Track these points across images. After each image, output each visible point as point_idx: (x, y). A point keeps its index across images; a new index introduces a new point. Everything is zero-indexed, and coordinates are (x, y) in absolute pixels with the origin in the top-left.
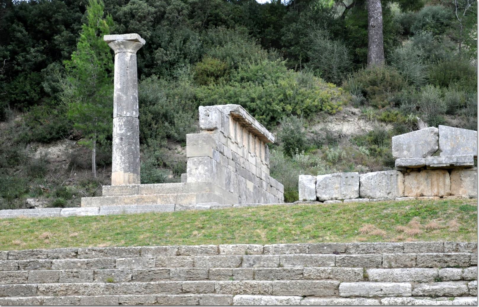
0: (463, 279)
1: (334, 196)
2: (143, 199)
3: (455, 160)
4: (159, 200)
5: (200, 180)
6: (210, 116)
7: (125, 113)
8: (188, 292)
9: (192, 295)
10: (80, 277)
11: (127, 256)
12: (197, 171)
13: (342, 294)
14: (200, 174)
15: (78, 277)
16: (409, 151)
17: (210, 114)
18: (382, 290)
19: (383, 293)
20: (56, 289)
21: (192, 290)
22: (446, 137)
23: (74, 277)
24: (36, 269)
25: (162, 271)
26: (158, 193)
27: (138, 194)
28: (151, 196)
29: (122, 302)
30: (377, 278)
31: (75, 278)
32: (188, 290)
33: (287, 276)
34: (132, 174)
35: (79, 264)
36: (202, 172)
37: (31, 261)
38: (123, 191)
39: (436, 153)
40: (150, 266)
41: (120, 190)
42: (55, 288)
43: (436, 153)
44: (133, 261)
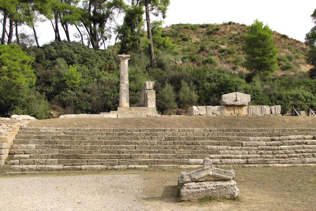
0: (279, 140)
2: (133, 112)
9: (190, 146)
18: (256, 144)
21: (191, 144)
27: (131, 110)
39: (236, 101)
43: (236, 101)
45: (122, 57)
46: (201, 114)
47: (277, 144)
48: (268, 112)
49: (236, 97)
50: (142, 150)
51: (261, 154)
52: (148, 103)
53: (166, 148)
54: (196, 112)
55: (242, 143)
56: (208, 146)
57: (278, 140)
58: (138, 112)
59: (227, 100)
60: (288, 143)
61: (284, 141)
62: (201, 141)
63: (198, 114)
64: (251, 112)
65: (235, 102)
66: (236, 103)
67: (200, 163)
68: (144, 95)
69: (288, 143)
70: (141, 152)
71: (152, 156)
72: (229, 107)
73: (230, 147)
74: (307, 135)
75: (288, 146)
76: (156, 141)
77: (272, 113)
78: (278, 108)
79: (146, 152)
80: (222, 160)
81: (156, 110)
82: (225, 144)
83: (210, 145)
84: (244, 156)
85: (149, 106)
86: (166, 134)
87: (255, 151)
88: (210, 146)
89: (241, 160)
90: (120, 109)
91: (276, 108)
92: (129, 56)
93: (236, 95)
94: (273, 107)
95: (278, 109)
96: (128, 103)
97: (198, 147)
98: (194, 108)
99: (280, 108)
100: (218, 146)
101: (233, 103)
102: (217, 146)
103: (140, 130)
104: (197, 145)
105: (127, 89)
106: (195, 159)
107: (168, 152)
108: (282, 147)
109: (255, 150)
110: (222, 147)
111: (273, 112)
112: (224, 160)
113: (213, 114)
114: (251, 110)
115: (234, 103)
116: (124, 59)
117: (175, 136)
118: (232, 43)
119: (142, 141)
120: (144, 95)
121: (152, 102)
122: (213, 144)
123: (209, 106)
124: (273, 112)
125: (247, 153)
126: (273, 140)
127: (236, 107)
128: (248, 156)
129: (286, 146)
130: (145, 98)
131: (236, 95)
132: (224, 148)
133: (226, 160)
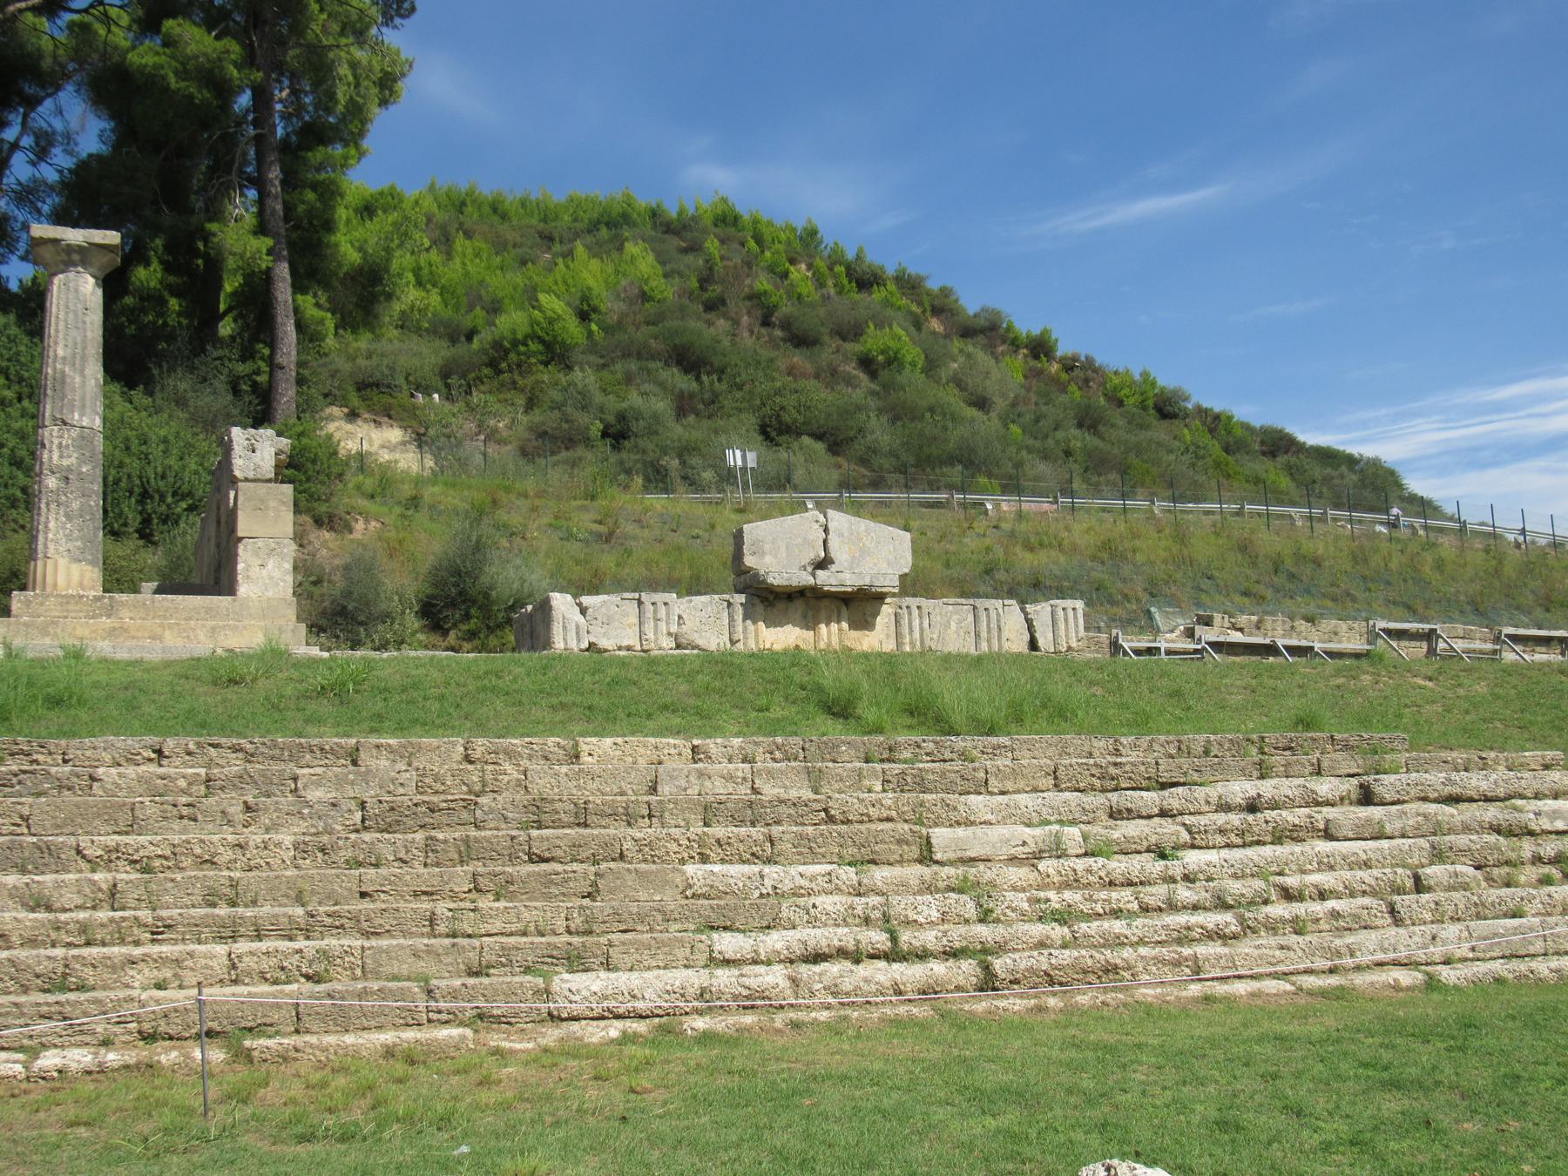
0: (1163, 814)
1: (625, 643)
2: (126, 630)
3: (867, 581)
4: (168, 634)
5: (270, 594)
6: (258, 453)
7: (76, 416)
8: (547, 860)
9: (559, 867)
10: (200, 817)
11: (316, 762)
12: (264, 572)
13: (938, 856)
14: (271, 578)
15: (195, 820)
16: (775, 556)
17: (257, 445)
18: (1024, 843)
19: (1027, 850)
20: (141, 853)
21: (559, 853)
22: (841, 535)
23: (182, 817)
24: (39, 795)
25: (452, 805)
26: (165, 617)
27: (109, 616)
28: (148, 623)
29: (370, 889)
30: (989, 817)
31: (185, 821)
32: (547, 855)
33: (789, 816)
34: (89, 568)
35: (182, 783)
36: (277, 574)
37: (25, 772)
38: (70, 607)
39: (823, 564)
40: (401, 791)
41: (61, 604)
42: (137, 850)
43: (823, 564)
44: (351, 777)
45: (56, 241)
46: (604, 643)
47: (1153, 839)
48: (1016, 642)
49: (825, 542)
50: (164, 913)
51: (1062, 917)
52: (240, 566)
53: (363, 895)
54: (572, 636)
55: (928, 838)
56: (690, 869)
57: (1156, 811)
58: (162, 626)
59: (768, 559)
60: (1222, 831)
61: (1192, 818)
62: (638, 835)
63: (585, 645)
64: (917, 635)
65: (819, 573)
66: (825, 579)
67: (641, 1005)
68: (219, 522)
69: (1222, 831)
70: (158, 932)
71: (248, 962)
72: (781, 605)
73: (848, 874)
74: (1319, 773)
75: (1225, 853)
76: (288, 840)
77: (1033, 645)
78: (1070, 613)
79: (196, 932)
80: (805, 970)
81: (291, 613)
82: (809, 851)
83: (704, 859)
84: (957, 935)
85: (243, 589)
86: (366, 777)
87: (1022, 895)
88: (708, 867)
89: (938, 968)
90: (28, 603)
91: (1061, 613)
92: (112, 237)
93: (826, 530)
94: (1041, 611)
95: (1071, 620)
96: (93, 563)
97: (617, 875)
98: (554, 603)
99: (1080, 613)
100: (767, 869)
101: (812, 581)
102: (756, 869)
103: (159, 752)
104: (605, 859)
105: (92, 472)
106: (603, 974)
107: (386, 922)
108: (1193, 859)
109: (1024, 890)
110: (794, 870)
111: (1045, 641)
112: (817, 969)
113: (678, 647)
114: (916, 623)
115: (813, 575)
116: (76, 257)
117: (435, 799)
118: (482, 696)
119: (176, 839)
120: (219, 522)
121: (270, 565)
122: (727, 851)
123: (659, 597)
124: (1041, 643)
125: (970, 910)
126: (1115, 814)
127: (825, 603)
128: (984, 932)
129: (1212, 856)
130: (224, 544)
131: (826, 530)
132: (803, 882)
133: (833, 969)
